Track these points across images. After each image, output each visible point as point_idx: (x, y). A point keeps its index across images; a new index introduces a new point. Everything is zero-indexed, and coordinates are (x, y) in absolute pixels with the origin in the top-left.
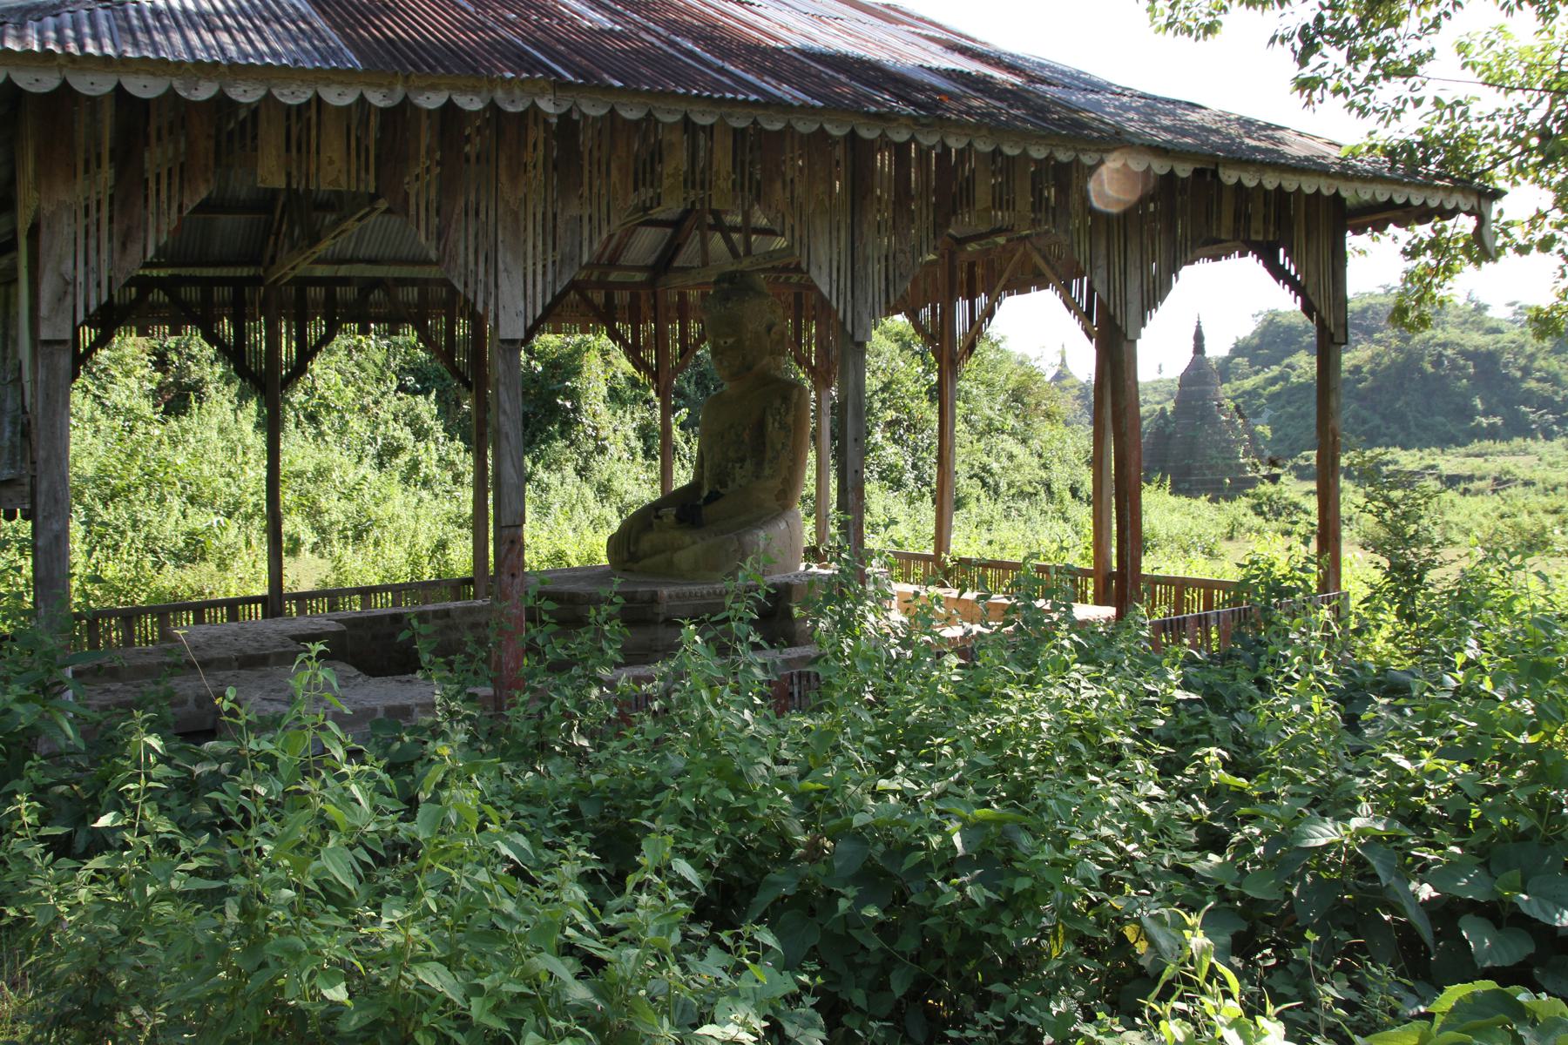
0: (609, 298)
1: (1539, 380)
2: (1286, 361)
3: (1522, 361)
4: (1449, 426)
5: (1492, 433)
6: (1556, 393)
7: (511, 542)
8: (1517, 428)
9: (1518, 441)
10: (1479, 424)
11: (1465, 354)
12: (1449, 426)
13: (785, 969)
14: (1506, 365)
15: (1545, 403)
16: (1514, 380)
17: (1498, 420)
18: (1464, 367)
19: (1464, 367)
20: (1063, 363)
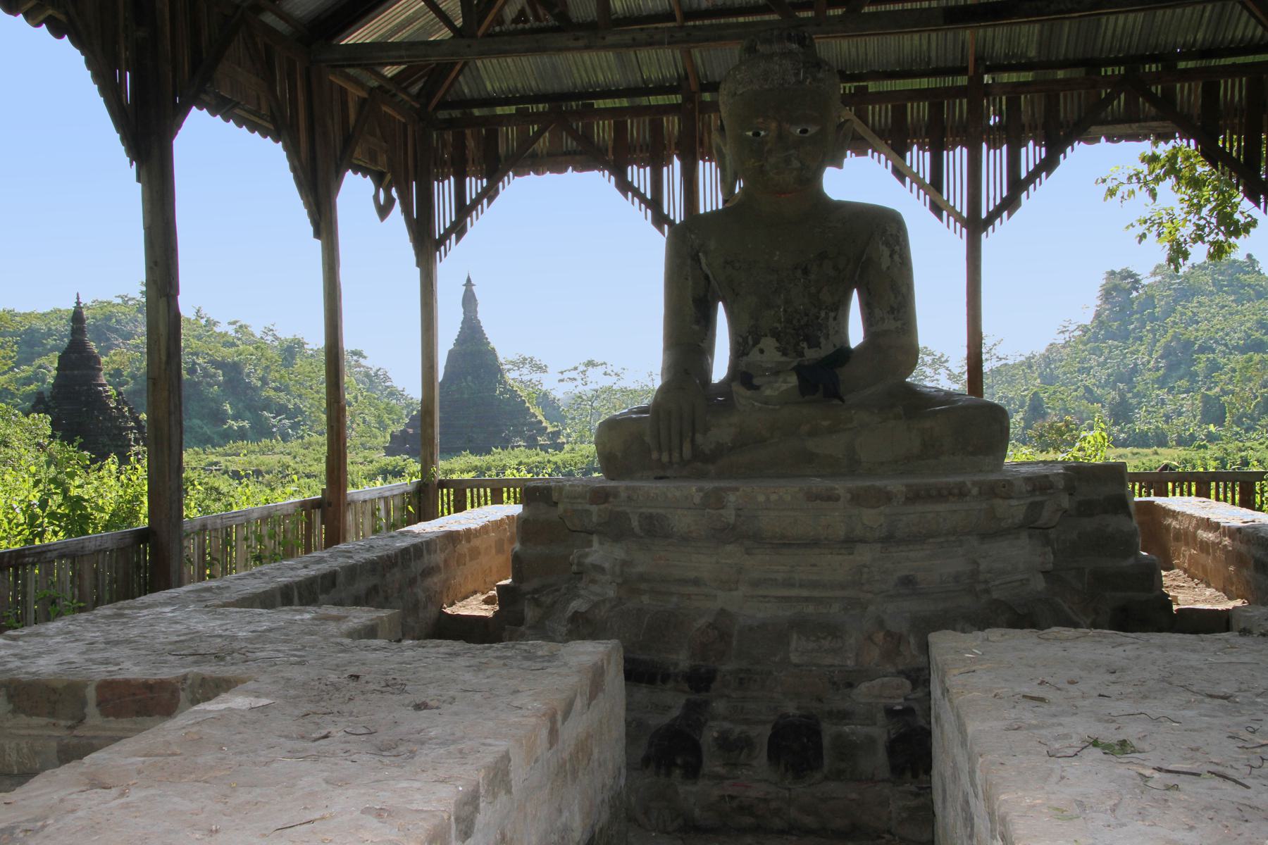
0: (1210, 92)
1: (276, 389)
2: (37, 362)
3: (260, 372)
4: (205, 428)
5: (242, 435)
6: (289, 401)
7: (671, 223)
8: (261, 431)
9: (265, 441)
10: (230, 427)
11: (213, 363)
12: (205, 428)
13: (405, 636)
14: (248, 375)
15: (281, 410)
16: (255, 389)
17: (246, 424)
18: (214, 375)
19: (214, 375)
20: (78, 303)
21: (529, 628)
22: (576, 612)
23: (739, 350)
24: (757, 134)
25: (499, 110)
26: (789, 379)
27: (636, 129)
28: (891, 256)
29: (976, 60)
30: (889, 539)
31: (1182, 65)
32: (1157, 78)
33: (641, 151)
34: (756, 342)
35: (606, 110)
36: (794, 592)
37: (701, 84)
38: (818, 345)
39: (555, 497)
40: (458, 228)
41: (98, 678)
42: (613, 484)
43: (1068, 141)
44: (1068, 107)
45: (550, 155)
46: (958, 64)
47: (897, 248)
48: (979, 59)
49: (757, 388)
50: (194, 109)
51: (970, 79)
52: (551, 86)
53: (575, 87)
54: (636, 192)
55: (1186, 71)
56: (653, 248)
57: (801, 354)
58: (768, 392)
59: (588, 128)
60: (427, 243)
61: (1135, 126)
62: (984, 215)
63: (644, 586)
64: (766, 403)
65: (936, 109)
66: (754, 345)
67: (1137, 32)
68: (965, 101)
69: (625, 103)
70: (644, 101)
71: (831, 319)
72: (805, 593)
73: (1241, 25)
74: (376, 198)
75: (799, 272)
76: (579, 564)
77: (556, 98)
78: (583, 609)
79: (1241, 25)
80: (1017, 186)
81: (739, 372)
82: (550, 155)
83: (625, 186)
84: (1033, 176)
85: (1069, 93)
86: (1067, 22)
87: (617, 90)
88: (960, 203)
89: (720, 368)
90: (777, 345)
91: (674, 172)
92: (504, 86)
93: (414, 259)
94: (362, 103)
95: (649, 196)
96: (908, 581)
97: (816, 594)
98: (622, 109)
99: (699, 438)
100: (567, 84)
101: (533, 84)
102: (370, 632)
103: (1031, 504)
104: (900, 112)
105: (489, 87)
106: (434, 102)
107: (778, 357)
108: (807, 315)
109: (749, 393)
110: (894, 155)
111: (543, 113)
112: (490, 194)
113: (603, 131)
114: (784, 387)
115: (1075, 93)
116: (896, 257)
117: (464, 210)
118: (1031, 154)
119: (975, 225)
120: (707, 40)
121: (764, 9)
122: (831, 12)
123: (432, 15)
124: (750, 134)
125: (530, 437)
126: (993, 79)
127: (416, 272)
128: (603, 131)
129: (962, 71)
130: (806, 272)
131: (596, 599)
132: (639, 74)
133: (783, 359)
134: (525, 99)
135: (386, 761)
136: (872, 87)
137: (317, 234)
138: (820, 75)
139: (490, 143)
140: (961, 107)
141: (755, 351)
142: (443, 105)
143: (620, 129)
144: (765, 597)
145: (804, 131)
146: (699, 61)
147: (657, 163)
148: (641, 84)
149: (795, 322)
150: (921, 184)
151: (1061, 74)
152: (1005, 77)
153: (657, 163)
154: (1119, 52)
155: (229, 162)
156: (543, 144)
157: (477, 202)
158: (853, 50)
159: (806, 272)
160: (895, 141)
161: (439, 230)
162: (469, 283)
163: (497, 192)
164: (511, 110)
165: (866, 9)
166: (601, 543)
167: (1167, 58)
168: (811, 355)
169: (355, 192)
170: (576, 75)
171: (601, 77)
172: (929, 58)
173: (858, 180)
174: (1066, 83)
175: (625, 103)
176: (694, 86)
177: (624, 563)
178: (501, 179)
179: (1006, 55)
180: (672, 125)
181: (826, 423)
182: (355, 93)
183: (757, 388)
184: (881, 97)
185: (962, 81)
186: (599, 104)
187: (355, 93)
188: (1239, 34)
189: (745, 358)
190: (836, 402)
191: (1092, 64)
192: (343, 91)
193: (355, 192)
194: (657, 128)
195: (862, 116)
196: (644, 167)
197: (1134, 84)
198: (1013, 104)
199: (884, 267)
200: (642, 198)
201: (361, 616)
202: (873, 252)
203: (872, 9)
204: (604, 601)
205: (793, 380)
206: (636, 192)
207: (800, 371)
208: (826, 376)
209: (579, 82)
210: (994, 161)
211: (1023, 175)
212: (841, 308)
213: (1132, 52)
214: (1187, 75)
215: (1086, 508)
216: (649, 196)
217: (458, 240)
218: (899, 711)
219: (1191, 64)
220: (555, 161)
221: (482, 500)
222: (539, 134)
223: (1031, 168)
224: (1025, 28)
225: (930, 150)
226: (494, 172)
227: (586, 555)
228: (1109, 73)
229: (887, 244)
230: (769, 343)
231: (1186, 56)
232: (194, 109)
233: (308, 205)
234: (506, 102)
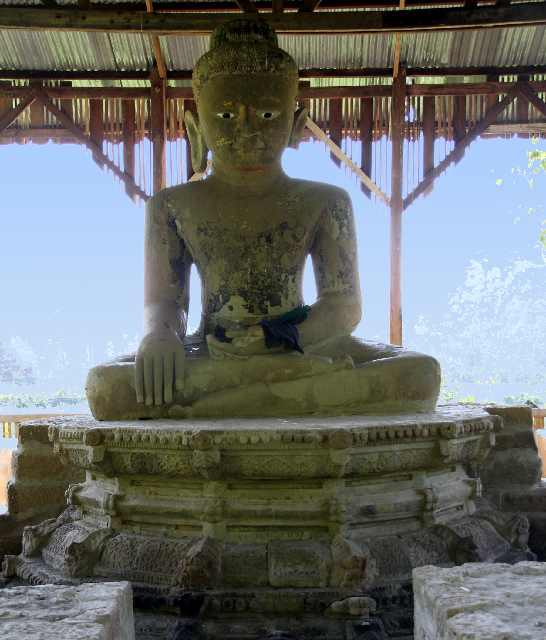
21: (27, 556)
22: (74, 544)
23: (211, 306)
24: (227, 116)
26: (256, 333)
27: (111, 109)
28: (340, 228)
29: (400, 64)
33: (115, 129)
34: (226, 301)
36: (271, 523)
37: (168, 72)
38: (279, 303)
39: (51, 437)
42: (105, 426)
43: (472, 136)
44: (475, 107)
46: (385, 66)
47: (345, 221)
48: (403, 63)
49: (229, 340)
51: (395, 80)
52: (33, 64)
53: (54, 66)
54: (111, 165)
56: (135, 218)
57: (265, 312)
58: (239, 344)
59: (67, 105)
61: (525, 126)
63: (136, 518)
64: (236, 354)
65: (367, 105)
66: (224, 303)
67: (529, 47)
68: (390, 99)
69: (98, 83)
70: (117, 83)
71: (290, 281)
72: (280, 523)
75: (263, 241)
76: (74, 498)
77: (37, 75)
78: (80, 539)
80: (430, 172)
81: (207, 326)
82: (32, 127)
83: (101, 159)
85: (473, 96)
86: (475, 32)
87: (93, 72)
89: (193, 324)
90: (245, 303)
91: (144, 148)
95: (122, 169)
96: (368, 511)
97: (290, 523)
99: (179, 384)
100: (46, 63)
101: (15, 60)
103: (467, 443)
104: (336, 107)
107: (245, 313)
108: (270, 277)
109: (222, 345)
110: (332, 143)
111: (25, 87)
113: (82, 108)
114: (252, 340)
115: (479, 96)
116: (345, 229)
118: (443, 146)
119: (398, 203)
120: (179, 28)
121: (232, 6)
122: (285, 11)
124: (221, 115)
125: (6, 373)
126: (413, 81)
128: (82, 108)
129: (388, 72)
130: (269, 240)
131: (91, 530)
132: (112, 59)
133: (251, 315)
136: (314, 82)
138: (282, 66)
141: (225, 308)
143: (95, 107)
144: (244, 527)
145: (268, 115)
146: (166, 49)
147: (129, 138)
148: (114, 68)
149: (259, 283)
151: (466, 79)
152: (424, 80)
153: (129, 138)
154: (514, 63)
158: (299, 49)
159: (269, 240)
165: (315, 11)
166: (94, 478)
168: (273, 311)
170: (55, 55)
171: (77, 59)
172: (362, 60)
173: (306, 161)
174: (472, 88)
176: (162, 73)
179: (424, 61)
180: (142, 106)
181: (288, 371)
183: (229, 340)
184: (321, 92)
185: (388, 81)
186: (77, 83)
189: (216, 314)
190: (296, 353)
191: (492, 72)
194: (128, 109)
196: (118, 143)
198: (429, 104)
199: (335, 237)
200: (116, 170)
202: (319, 223)
203: (318, 11)
204: (99, 533)
205: (260, 333)
206: (111, 165)
207: (265, 326)
208: (284, 331)
209: (57, 62)
210: (414, 150)
212: (296, 270)
213: (524, 63)
216: (122, 169)
218: (366, 626)
222: (22, 107)
224: (441, 35)
225: (454, 140)
227: (79, 489)
228: (506, 80)
229: (337, 218)
230: (237, 301)
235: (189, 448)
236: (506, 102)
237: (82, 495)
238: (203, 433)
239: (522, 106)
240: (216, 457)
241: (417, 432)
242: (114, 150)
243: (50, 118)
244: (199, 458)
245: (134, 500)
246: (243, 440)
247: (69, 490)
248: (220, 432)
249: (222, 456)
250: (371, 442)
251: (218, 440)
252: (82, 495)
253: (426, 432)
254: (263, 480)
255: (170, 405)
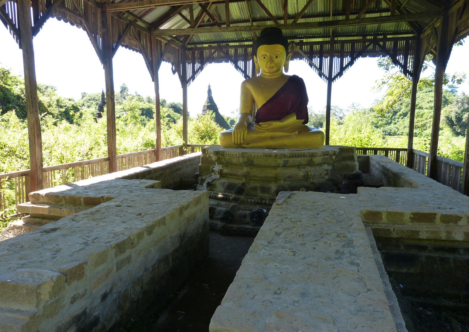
0: (396, 44)
25: (204, 45)
30: (285, 166)
31: (389, 37)
32: (381, 40)
35: (233, 46)
40: (193, 78)
41: (84, 196)
43: (358, 56)
45: (217, 58)
50: (120, 46)
52: (218, 39)
54: (240, 69)
55: (390, 38)
59: (385, 44)
60: (185, 82)
62: (333, 77)
69: (238, 44)
73: (404, 26)
74: (172, 69)
76: (212, 170)
79: (404, 26)
80: (342, 69)
83: (237, 67)
84: (347, 66)
88: (327, 74)
92: (205, 39)
93: (181, 86)
94: (166, 44)
98: (237, 46)
102: (152, 187)
104: (311, 48)
105: (201, 39)
106: (187, 43)
112: (201, 68)
113: (232, 51)
117: (195, 73)
119: (330, 80)
123: (184, 20)
127: (181, 90)
128: (232, 51)
134: (211, 42)
135: (413, 190)
136: (305, 40)
137: (153, 81)
139: (201, 54)
140: (327, 47)
142: (189, 44)
143: (236, 51)
147: (245, 60)
150: (316, 68)
155: (129, 62)
156: (216, 54)
157: (198, 70)
160: (310, 55)
161: (188, 78)
162: (209, 86)
163: (203, 68)
164: (207, 45)
167: (385, 34)
169: (166, 68)
171: (231, 37)
175: (238, 44)
177: (221, 170)
178: (204, 64)
182: (164, 42)
184: (307, 43)
185: (328, 39)
186: (231, 44)
187: (164, 42)
188: (404, 29)
192: (161, 42)
193: (166, 68)
195: (301, 48)
197: (375, 42)
200: (242, 70)
201: (151, 182)
211: (344, 66)
214: (390, 39)
215: (344, 159)
217: (193, 81)
219: (391, 36)
220: (219, 60)
221: (25, 200)
222: (215, 52)
223: (346, 64)
226: (203, 62)
227: (213, 167)
231: (390, 34)
232: (120, 46)
233: (150, 73)
234: (206, 43)
235: (239, 157)
236: (369, 45)
237: (214, 169)
238: (242, 153)
239: (374, 47)
240: (246, 160)
241: (305, 155)
242: (316, 61)
243: (222, 54)
244: (241, 160)
245: (225, 171)
246: (253, 155)
247: (211, 168)
248: (247, 153)
249: (248, 160)
250: (290, 157)
251: (246, 155)
252: (214, 169)
253: (308, 155)
254: (259, 166)
255: (242, 144)
